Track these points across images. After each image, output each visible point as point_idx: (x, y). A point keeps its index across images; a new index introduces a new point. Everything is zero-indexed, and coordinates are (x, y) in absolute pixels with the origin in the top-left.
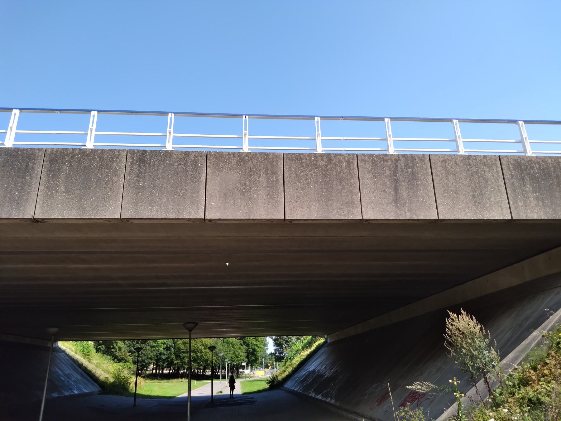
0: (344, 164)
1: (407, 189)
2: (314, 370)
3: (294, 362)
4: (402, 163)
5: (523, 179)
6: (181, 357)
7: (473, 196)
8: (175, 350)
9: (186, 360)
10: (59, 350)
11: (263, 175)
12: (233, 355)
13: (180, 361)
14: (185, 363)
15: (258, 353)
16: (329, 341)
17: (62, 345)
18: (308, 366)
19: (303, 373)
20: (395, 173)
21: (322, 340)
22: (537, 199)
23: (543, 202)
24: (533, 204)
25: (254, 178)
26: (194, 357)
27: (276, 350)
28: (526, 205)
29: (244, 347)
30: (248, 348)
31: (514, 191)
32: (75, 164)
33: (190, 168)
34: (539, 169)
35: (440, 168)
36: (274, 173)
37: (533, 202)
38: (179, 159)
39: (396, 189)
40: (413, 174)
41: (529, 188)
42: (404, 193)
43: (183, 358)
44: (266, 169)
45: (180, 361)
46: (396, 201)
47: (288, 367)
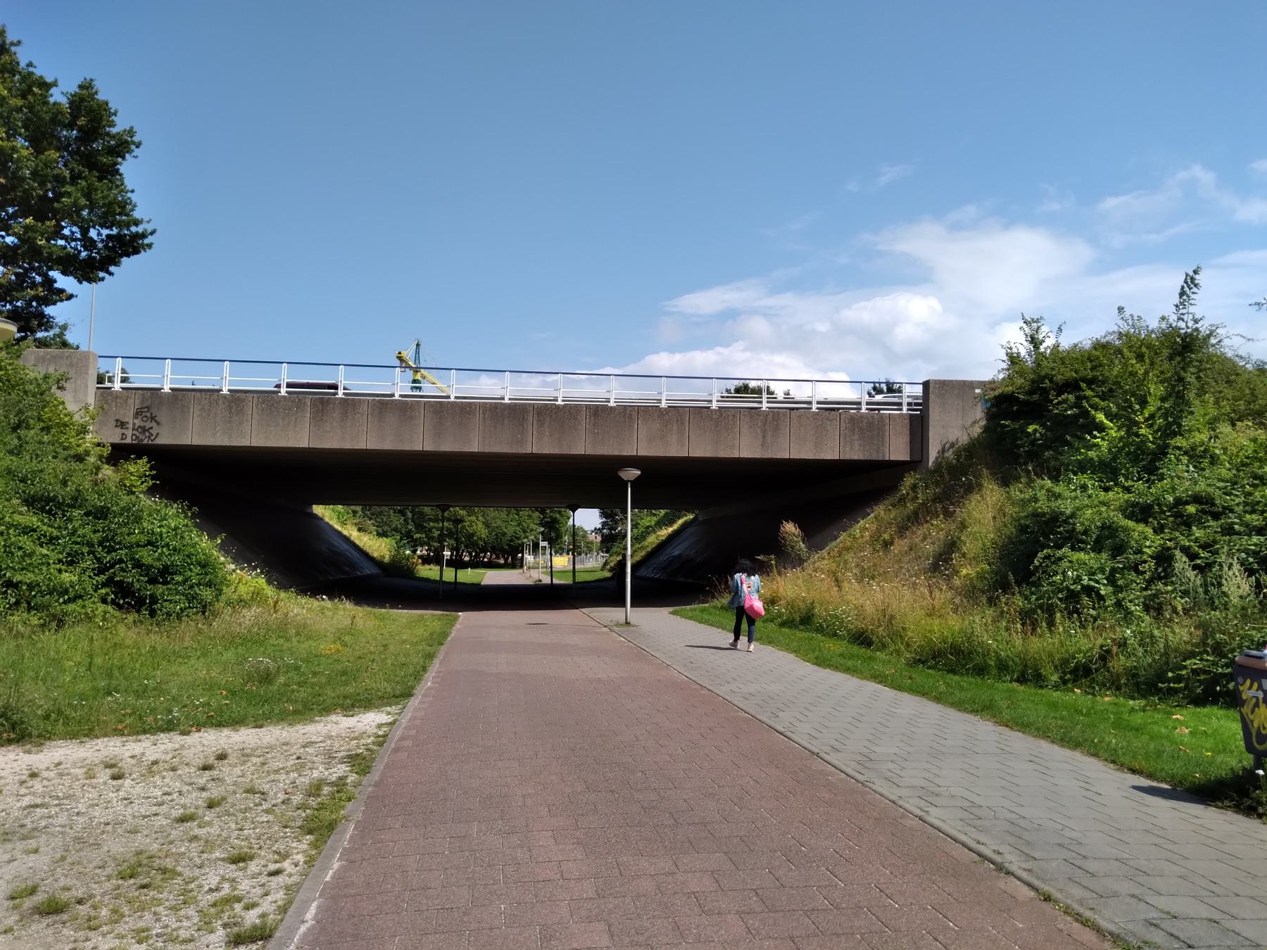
0: (731, 418)
1: (772, 436)
2: (680, 555)
3: (645, 543)
4: (770, 417)
5: (853, 430)
6: (426, 527)
7: (816, 443)
8: (413, 516)
9: (436, 533)
10: (315, 517)
11: (675, 425)
12: (518, 528)
13: (424, 535)
14: (433, 538)
15: (561, 525)
16: (700, 518)
17: (318, 510)
18: (672, 547)
19: (663, 558)
20: (765, 425)
21: (691, 517)
22: (860, 445)
23: (864, 447)
24: (856, 449)
25: (670, 426)
26: (450, 529)
27: (604, 524)
28: (851, 449)
29: (537, 514)
30: (544, 517)
31: (845, 439)
32: (554, 416)
33: (627, 420)
34: (867, 423)
35: (795, 422)
36: (683, 424)
37: (856, 444)
38: (620, 413)
39: (764, 437)
40: (777, 425)
41: (856, 437)
42: (769, 439)
43: (430, 530)
44: (678, 421)
45: (424, 535)
46: (763, 445)
47: (962, 523)
